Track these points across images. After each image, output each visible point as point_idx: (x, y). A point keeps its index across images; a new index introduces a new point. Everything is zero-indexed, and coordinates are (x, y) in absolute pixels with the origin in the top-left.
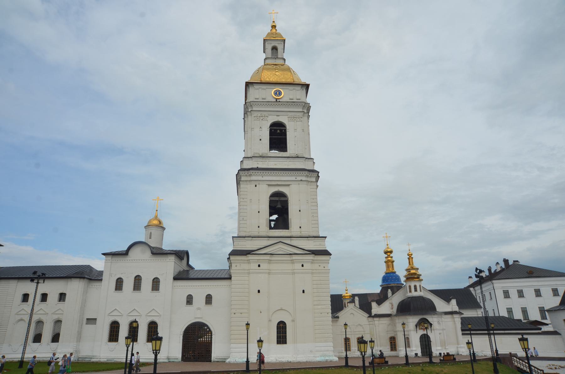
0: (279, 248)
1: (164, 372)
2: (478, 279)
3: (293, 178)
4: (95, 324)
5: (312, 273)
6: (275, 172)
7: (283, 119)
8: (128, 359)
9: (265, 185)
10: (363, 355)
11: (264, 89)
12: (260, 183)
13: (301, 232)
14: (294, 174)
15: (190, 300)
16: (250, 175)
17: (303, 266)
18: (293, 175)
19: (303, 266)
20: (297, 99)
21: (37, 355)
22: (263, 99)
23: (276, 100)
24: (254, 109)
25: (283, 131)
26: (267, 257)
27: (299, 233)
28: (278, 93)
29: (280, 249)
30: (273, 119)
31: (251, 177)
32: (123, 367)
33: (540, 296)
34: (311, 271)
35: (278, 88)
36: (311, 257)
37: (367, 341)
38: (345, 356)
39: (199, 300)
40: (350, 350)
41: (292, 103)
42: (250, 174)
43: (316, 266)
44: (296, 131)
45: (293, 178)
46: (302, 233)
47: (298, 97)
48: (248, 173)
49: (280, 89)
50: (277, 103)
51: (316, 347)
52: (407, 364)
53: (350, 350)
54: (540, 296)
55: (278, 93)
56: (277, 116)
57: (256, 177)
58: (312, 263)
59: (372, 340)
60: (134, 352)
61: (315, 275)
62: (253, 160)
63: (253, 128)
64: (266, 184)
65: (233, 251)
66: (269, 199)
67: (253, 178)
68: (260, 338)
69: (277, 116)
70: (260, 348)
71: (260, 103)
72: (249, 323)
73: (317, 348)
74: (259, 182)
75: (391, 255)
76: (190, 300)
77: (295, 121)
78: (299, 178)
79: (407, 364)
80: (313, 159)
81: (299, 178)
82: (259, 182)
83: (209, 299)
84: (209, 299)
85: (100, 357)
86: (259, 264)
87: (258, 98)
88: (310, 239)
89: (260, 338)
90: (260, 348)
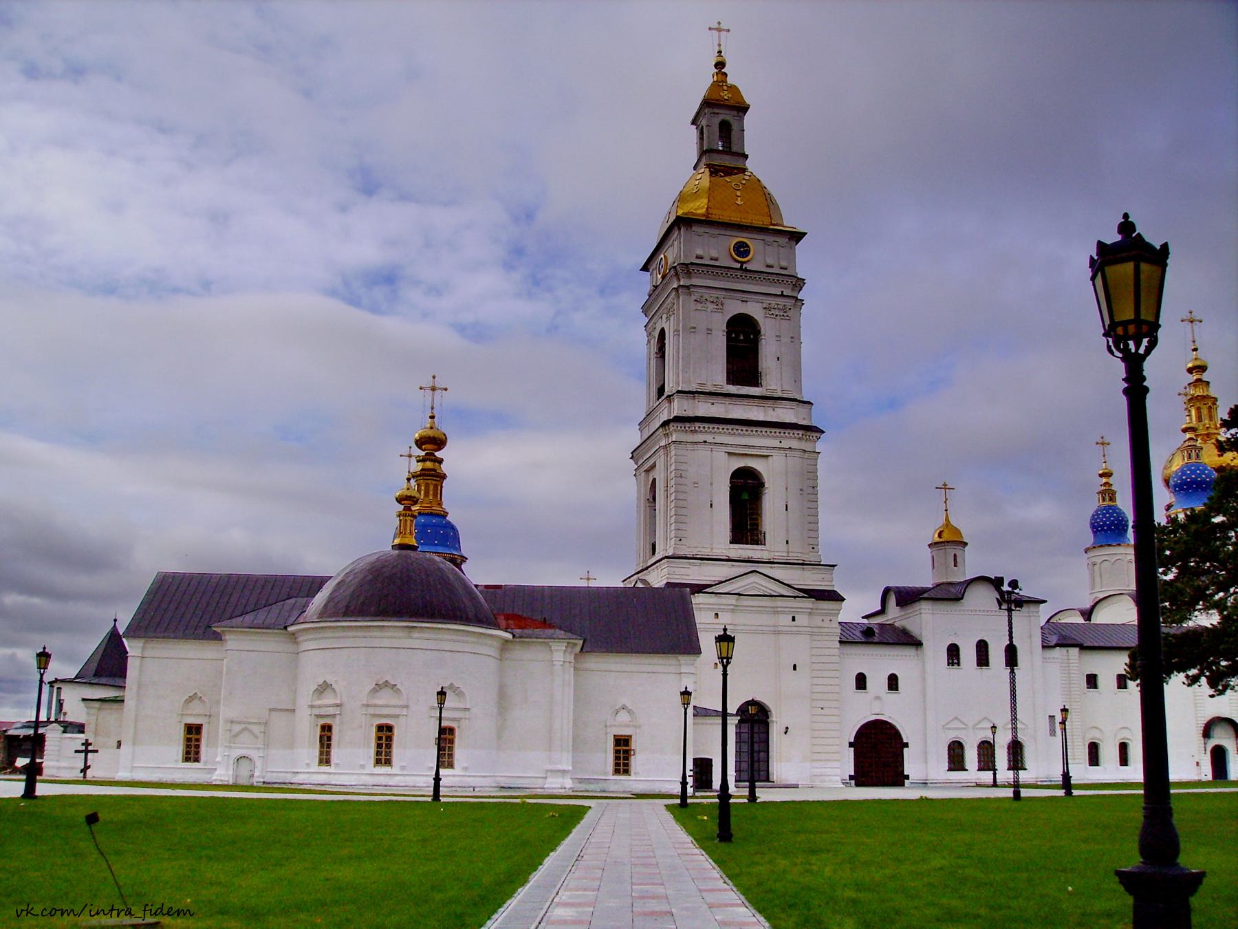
0: (751, 583)
2: (1230, 663)
3: (775, 443)
4: (1051, 734)
5: (812, 634)
7: (754, 310)
11: (713, 236)
13: (788, 552)
14: (768, 433)
15: (861, 682)
17: (794, 619)
18: (770, 435)
19: (794, 619)
22: (768, 266)
26: (732, 600)
27: (709, 550)
28: (742, 250)
29: (754, 585)
30: (736, 307)
33: (1095, 686)
34: (809, 629)
35: (744, 238)
36: (809, 603)
39: (876, 682)
40: (451, 766)
42: (693, 428)
43: (817, 621)
44: (710, 332)
45: (775, 443)
47: (714, 254)
48: (689, 427)
53: (451, 766)
54: (1095, 686)
55: (742, 250)
56: (742, 301)
57: (706, 434)
58: (733, 611)
61: (814, 637)
66: (730, 483)
69: (742, 301)
71: (705, 269)
73: (815, 770)
74: (712, 447)
76: (861, 682)
78: (786, 443)
80: (812, 404)
81: (786, 443)
83: (893, 683)
84: (893, 683)
88: (807, 568)
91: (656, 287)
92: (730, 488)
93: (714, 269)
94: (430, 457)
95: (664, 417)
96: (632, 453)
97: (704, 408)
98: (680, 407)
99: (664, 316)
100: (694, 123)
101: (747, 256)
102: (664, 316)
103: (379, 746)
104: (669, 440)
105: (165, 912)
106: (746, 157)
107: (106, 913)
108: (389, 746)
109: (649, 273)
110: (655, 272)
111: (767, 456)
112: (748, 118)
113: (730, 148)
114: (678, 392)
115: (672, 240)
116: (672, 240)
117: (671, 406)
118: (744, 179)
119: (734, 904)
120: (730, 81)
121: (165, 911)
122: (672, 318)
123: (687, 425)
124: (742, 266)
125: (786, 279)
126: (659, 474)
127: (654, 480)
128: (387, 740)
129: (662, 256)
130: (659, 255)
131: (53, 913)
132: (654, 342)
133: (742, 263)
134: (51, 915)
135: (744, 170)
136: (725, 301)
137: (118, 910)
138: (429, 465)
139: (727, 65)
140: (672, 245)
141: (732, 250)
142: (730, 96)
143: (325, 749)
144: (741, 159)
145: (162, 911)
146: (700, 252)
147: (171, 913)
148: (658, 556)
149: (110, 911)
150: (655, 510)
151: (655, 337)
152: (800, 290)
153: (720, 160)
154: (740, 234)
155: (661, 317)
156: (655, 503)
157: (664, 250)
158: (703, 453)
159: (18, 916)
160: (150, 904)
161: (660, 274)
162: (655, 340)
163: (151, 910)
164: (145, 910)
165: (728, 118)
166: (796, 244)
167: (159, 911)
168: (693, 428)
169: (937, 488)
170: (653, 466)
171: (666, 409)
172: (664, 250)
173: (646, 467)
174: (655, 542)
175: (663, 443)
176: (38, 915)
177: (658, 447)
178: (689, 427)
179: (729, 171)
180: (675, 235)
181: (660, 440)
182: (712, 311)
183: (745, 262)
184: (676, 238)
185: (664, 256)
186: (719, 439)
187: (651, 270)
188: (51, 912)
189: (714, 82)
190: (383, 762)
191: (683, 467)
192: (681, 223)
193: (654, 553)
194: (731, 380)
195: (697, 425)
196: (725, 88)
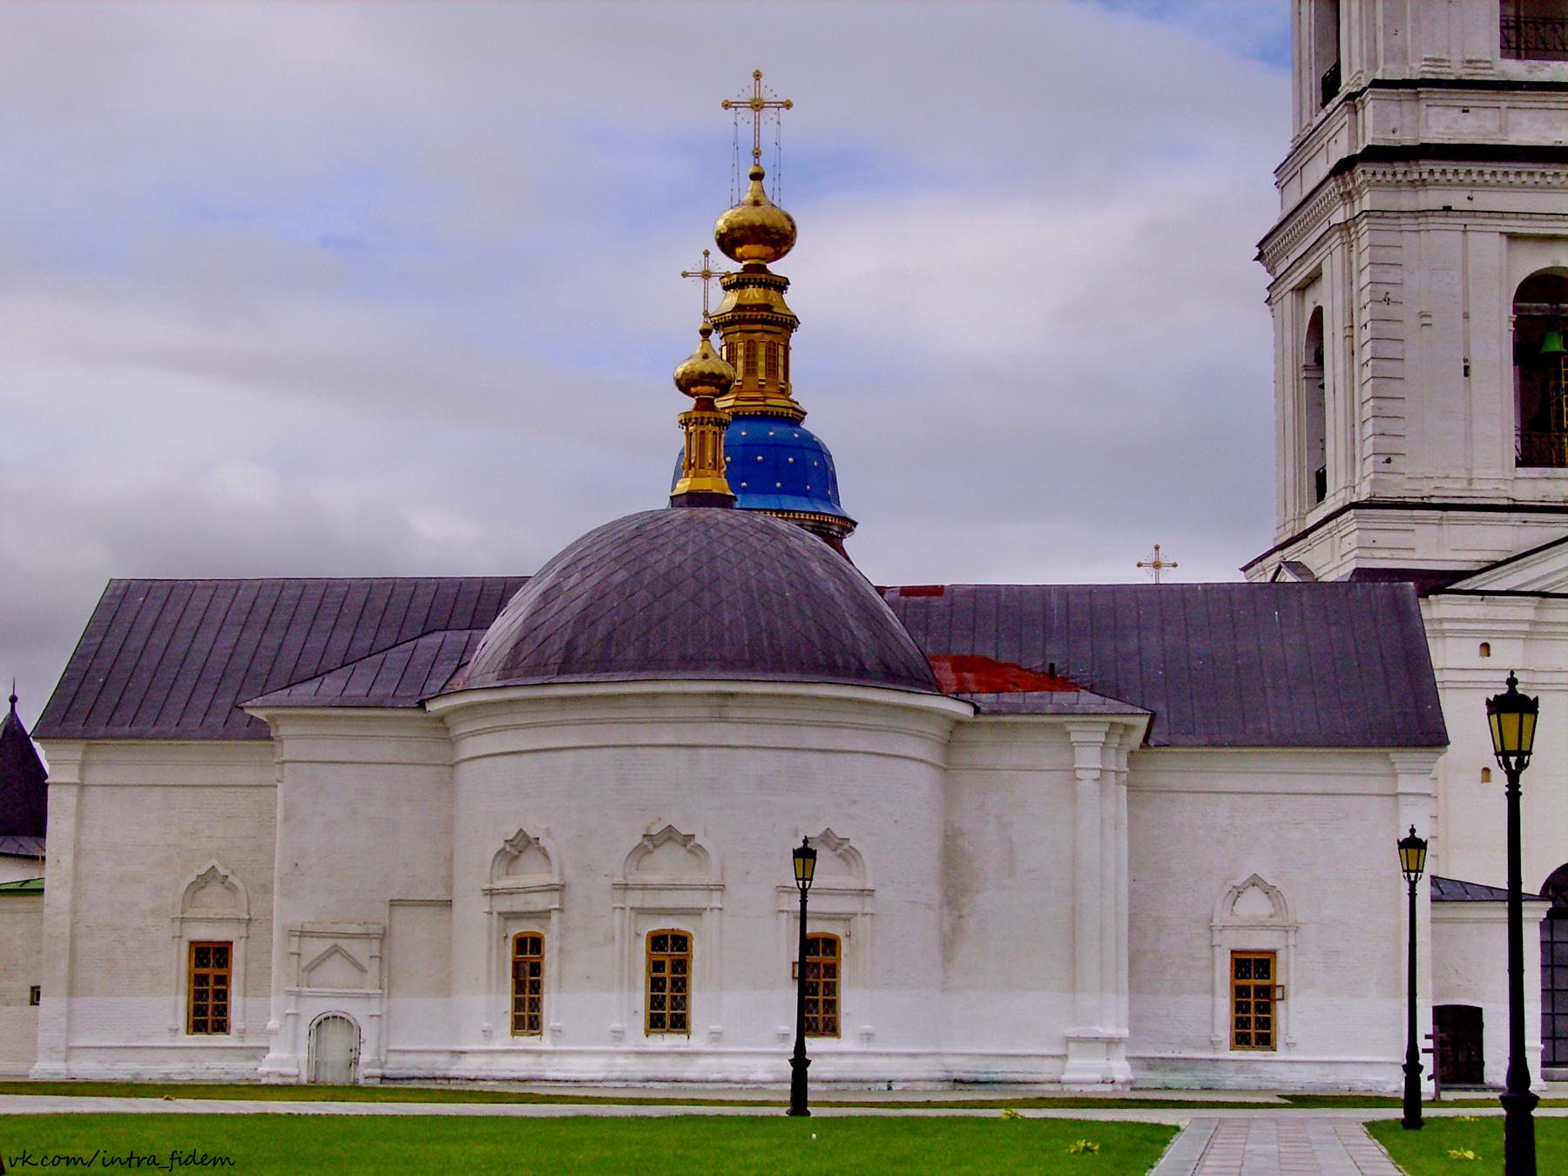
8: (802, 514)
10: (1413, 879)
12: (1468, 228)
32: (23, 999)
37: (1424, 841)
38: (1105, 1045)
42: (1416, 176)
46: (1476, 485)
59: (1417, 835)
60: (738, 109)
64: (1501, 233)
68: (1413, 831)
70: (1413, 875)
74: (1466, 221)
85: (1140, 788)
86: (526, 1041)
89: (1413, 831)
90: (1413, 875)
103: (656, 984)
104: (1352, 210)
108: (681, 985)
114: (1376, 84)
121: (198, 1160)
127: (1318, 313)
128: (674, 970)
143: (211, 1002)
147: (204, 1162)
163: (180, 1158)
167: (191, 1158)
173: (1297, 278)
176: (37, 1164)
178: (1405, 174)
181: (1329, 209)
188: (53, 1161)
190: (821, 1026)
191: (1394, 275)
193: (1321, 491)
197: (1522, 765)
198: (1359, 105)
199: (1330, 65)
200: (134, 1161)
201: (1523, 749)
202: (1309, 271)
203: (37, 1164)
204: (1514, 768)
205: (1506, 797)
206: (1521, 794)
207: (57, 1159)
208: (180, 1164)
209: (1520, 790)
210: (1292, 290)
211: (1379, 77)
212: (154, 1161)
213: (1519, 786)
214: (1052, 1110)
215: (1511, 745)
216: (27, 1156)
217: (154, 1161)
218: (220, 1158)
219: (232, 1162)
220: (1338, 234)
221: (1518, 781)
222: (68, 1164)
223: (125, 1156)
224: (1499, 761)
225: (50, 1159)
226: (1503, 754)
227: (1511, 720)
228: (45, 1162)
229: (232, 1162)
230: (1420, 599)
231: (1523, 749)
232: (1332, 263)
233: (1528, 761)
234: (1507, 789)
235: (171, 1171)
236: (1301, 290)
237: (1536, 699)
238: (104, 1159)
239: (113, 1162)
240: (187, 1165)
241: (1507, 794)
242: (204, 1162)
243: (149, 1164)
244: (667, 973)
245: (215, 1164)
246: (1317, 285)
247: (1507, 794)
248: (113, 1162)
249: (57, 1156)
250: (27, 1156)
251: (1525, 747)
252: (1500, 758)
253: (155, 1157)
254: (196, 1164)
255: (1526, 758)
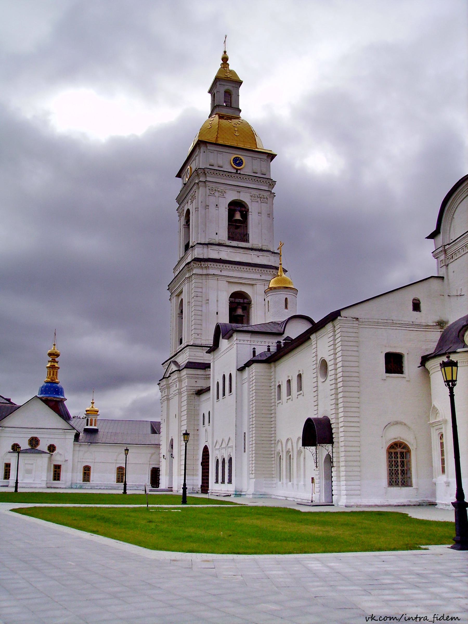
1: (324, 497)
6: (228, 265)
7: (245, 197)
9: (225, 282)
16: (207, 268)
20: (219, 167)
21: (214, 482)
23: (237, 171)
24: (208, 179)
25: (244, 212)
30: (232, 196)
31: (208, 270)
41: (255, 178)
42: (207, 266)
47: (221, 163)
48: (204, 265)
49: (239, 156)
50: (238, 175)
51: (41, 483)
52: (184, 500)
55: (238, 162)
57: (214, 269)
62: (209, 248)
63: (208, 206)
64: (227, 281)
65: (189, 363)
67: (211, 271)
72: (128, 448)
75: (57, 359)
77: (260, 202)
79: (184, 500)
82: (217, 278)
87: (265, 174)
91: (185, 184)
92: (229, 303)
93: (219, 172)
94: (54, 361)
95: (189, 260)
96: (168, 286)
97: (213, 253)
98: (198, 252)
99: (190, 201)
100: (209, 92)
101: (241, 166)
102: (190, 201)
104: (190, 274)
105: (445, 618)
106: (240, 111)
107: (413, 619)
109: (181, 179)
110: (184, 178)
111: (253, 285)
112: (242, 90)
113: (231, 106)
114: (198, 244)
115: (195, 156)
116: (195, 156)
117: (193, 252)
118: (239, 121)
119: (213, 452)
120: (231, 68)
121: (445, 618)
122: (194, 202)
123: (203, 263)
124: (237, 171)
125: (264, 180)
126: (184, 296)
127: (182, 300)
129: (189, 167)
130: (187, 167)
131: (386, 618)
132: (183, 218)
133: (237, 170)
134: (384, 620)
135: (239, 118)
136: (226, 191)
137: (420, 617)
138: (53, 364)
139: (229, 60)
140: (195, 159)
141: (232, 163)
142: (231, 76)
144: (238, 112)
145: (443, 618)
146: (212, 162)
147: (448, 619)
148: (183, 346)
149: (415, 618)
150: (182, 318)
151: (183, 216)
152: (273, 188)
153: (224, 112)
154: (237, 153)
155: (188, 203)
156: (182, 315)
157: (190, 164)
158: (212, 282)
159: (367, 621)
160: (437, 615)
161: (187, 178)
162: (183, 218)
163: (437, 617)
164: (434, 618)
165: (230, 88)
166: (271, 161)
167: (442, 618)
168: (207, 266)
169: (329, 347)
170: (181, 292)
171: (190, 255)
172: (190, 164)
173: (177, 293)
174: (182, 338)
175: (187, 276)
176: (377, 620)
177: (185, 278)
179: (230, 118)
180: (197, 153)
181: (185, 274)
182: (219, 197)
183: (240, 169)
184: (198, 154)
185: (190, 167)
186: (224, 273)
187: (182, 177)
188: (384, 619)
189: (221, 68)
192: (200, 144)
193: (181, 343)
194: (230, 238)
195: (209, 263)
196: (228, 71)
197: (454, 385)
198: (194, 249)
199: (186, 242)
200: (418, 619)
201: (454, 379)
202: (179, 291)
203: (377, 620)
204: (451, 386)
205: (449, 397)
206: (454, 395)
207: (386, 618)
208: (437, 620)
209: (454, 394)
210: (176, 296)
211: (199, 242)
212: (426, 619)
213: (454, 392)
214: (25, 492)
215: (449, 378)
216: (373, 617)
217: (426, 619)
218: (454, 618)
219: (459, 619)
220: (187, 280)
221: (453, 390)
222: (390, 620)
223: (414, 616)
224: (445, 384)
225: (383, 618)
226: (447, 382)
227: (448, 369)
228: (381, 619)
229: (459, 619)
230: (256, 355)
231: (454, 379)
232: (185, 288)
233: (456, 383)
234: (449, 394)
235: (433, 623)
236: (178, 295)
237: (457, 362)
238: (405, 617)
239: (409, 619)
240: (440, 620)
241: (449, 395)
242: (448, 619)
243: (424, 620)
244: (57, 475)
245: (452, 620)
246: (182, 294)
247: (449, 395)
248: (409, 619)
249: (386, 617)
250: (373, 617)
251: (454, 379)
252: (446, 383)
253: (427, 617)
254: (444, 620)
255: (455, 382)
